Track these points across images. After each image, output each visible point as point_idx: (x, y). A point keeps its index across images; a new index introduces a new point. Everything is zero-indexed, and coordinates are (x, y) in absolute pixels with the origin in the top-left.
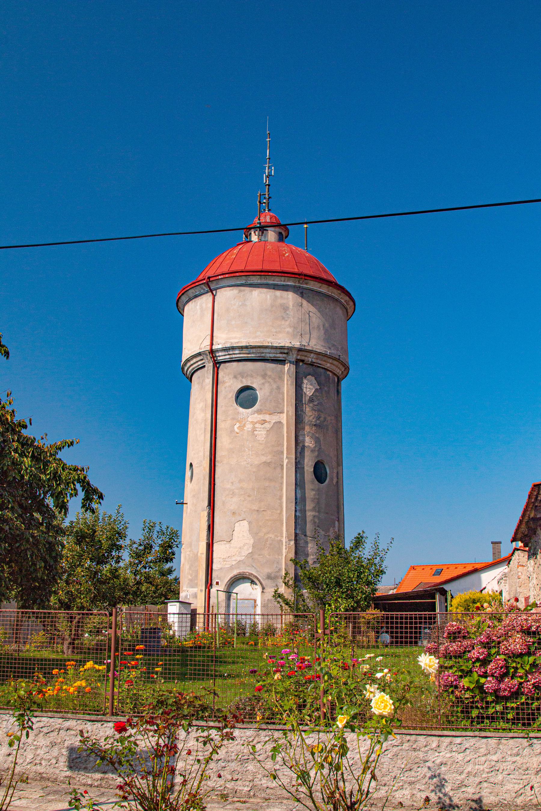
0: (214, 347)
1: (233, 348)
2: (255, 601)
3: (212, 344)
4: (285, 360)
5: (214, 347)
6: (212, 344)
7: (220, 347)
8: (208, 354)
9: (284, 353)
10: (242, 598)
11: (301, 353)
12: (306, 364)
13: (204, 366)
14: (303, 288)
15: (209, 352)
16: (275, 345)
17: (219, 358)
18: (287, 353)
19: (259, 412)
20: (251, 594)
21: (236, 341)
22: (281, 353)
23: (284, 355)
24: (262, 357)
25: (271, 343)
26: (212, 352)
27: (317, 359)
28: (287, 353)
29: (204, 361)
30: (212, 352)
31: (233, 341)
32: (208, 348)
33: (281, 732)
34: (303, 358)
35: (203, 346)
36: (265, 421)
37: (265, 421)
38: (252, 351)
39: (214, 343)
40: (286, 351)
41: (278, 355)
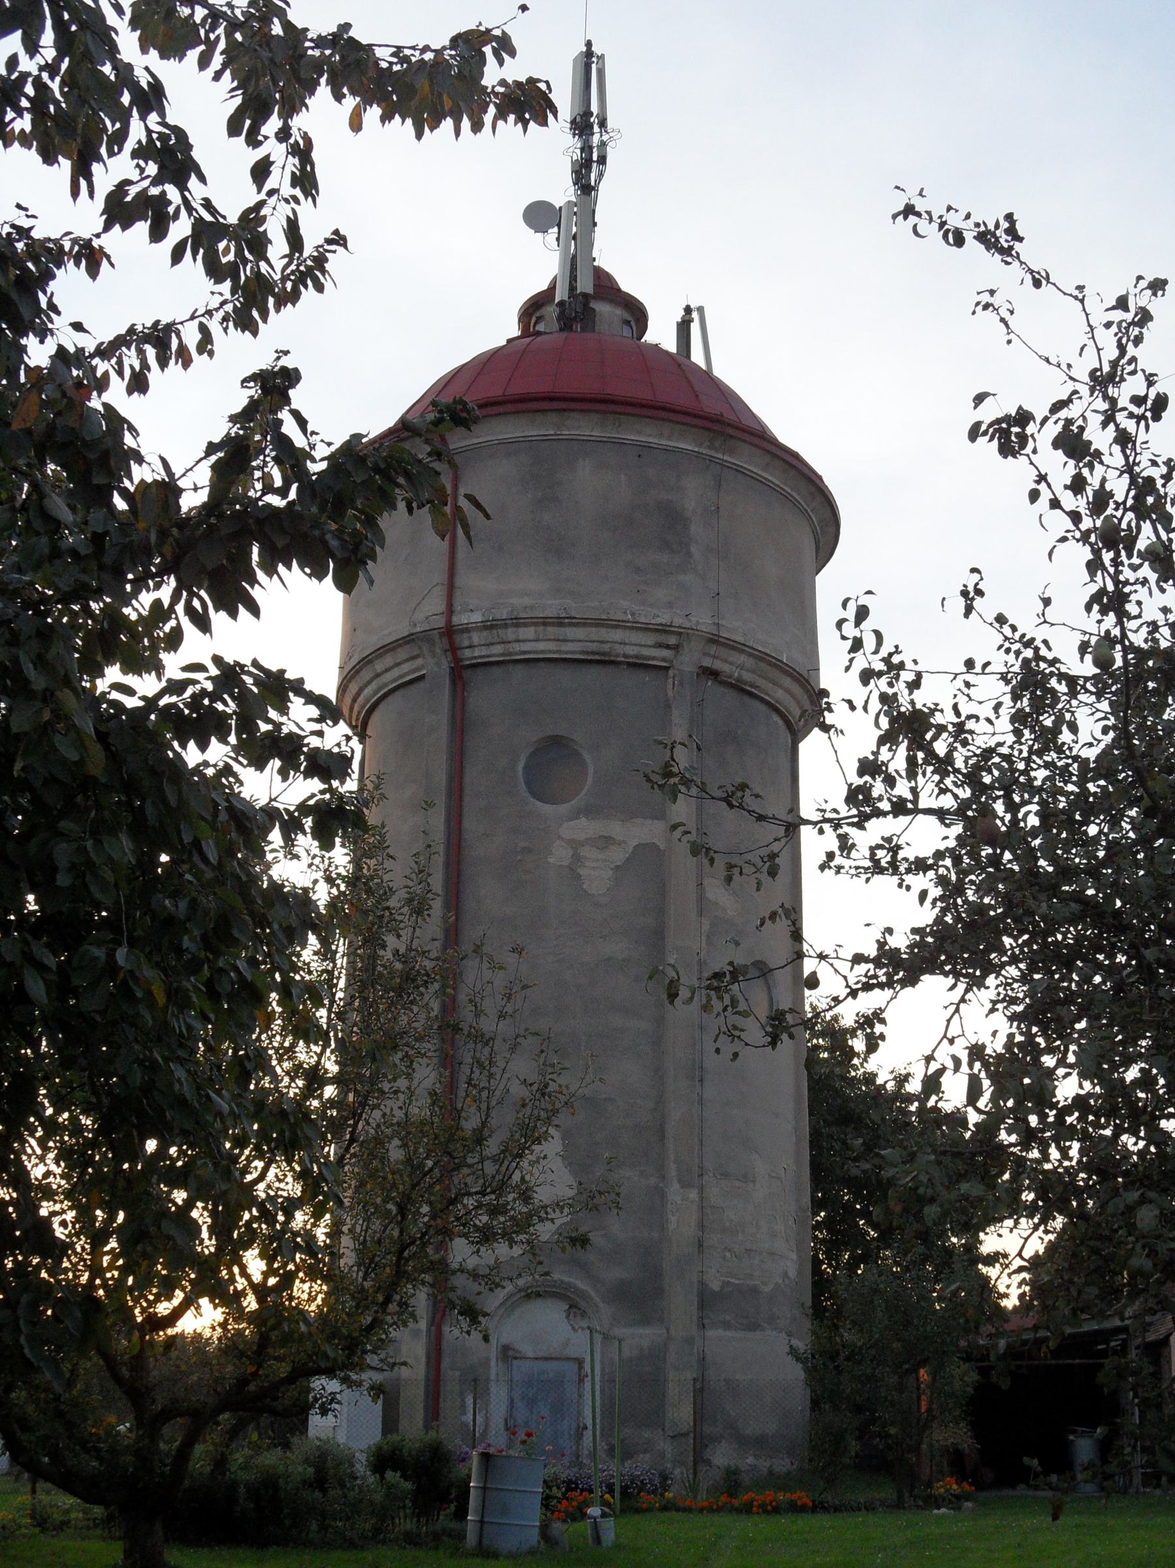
0: (460, 619)
1: (517, 622)
2: (580, 1362)
3: (450, 611)
4: (667, 669)
5: (456, 620)
6: (450, 611)
7: (477, 617)
8: (437, 638)
9: (668, 647)
10: (540, 1354)
11: (713, 649)
12: (721, 683)
13: (422, 677)
14: (723, 465)
15: (442, 635)
16: (643, 620)
17: (467, 653)
18: (676, 648)
19: (588, 811)
20: (566, 1343)
21: (527, 601)
22: (660, 645)
23: (666, 653)
24: (603, 654)
25: (633, 614)
26: (450, 632)
27: (753, 672)
28: (676, 648)
29: (419, 662)
30: (450, 632)
31: (516, 601)
32: (440, 622)
33: (706, 882)
34: (718, 665)
35: (419, 616)
36: (606, 841)
37: (606, 841)
38: (570, 632)
39: (457, 607)
40: (672, 640)
41: (647, 652)
